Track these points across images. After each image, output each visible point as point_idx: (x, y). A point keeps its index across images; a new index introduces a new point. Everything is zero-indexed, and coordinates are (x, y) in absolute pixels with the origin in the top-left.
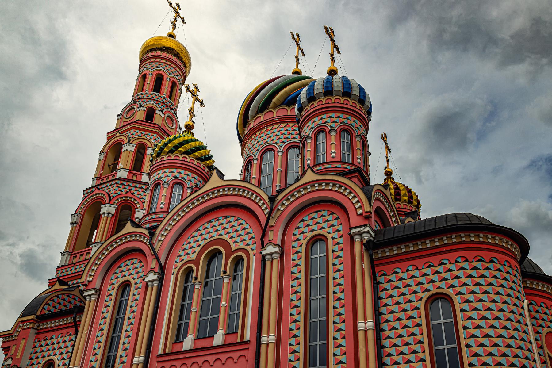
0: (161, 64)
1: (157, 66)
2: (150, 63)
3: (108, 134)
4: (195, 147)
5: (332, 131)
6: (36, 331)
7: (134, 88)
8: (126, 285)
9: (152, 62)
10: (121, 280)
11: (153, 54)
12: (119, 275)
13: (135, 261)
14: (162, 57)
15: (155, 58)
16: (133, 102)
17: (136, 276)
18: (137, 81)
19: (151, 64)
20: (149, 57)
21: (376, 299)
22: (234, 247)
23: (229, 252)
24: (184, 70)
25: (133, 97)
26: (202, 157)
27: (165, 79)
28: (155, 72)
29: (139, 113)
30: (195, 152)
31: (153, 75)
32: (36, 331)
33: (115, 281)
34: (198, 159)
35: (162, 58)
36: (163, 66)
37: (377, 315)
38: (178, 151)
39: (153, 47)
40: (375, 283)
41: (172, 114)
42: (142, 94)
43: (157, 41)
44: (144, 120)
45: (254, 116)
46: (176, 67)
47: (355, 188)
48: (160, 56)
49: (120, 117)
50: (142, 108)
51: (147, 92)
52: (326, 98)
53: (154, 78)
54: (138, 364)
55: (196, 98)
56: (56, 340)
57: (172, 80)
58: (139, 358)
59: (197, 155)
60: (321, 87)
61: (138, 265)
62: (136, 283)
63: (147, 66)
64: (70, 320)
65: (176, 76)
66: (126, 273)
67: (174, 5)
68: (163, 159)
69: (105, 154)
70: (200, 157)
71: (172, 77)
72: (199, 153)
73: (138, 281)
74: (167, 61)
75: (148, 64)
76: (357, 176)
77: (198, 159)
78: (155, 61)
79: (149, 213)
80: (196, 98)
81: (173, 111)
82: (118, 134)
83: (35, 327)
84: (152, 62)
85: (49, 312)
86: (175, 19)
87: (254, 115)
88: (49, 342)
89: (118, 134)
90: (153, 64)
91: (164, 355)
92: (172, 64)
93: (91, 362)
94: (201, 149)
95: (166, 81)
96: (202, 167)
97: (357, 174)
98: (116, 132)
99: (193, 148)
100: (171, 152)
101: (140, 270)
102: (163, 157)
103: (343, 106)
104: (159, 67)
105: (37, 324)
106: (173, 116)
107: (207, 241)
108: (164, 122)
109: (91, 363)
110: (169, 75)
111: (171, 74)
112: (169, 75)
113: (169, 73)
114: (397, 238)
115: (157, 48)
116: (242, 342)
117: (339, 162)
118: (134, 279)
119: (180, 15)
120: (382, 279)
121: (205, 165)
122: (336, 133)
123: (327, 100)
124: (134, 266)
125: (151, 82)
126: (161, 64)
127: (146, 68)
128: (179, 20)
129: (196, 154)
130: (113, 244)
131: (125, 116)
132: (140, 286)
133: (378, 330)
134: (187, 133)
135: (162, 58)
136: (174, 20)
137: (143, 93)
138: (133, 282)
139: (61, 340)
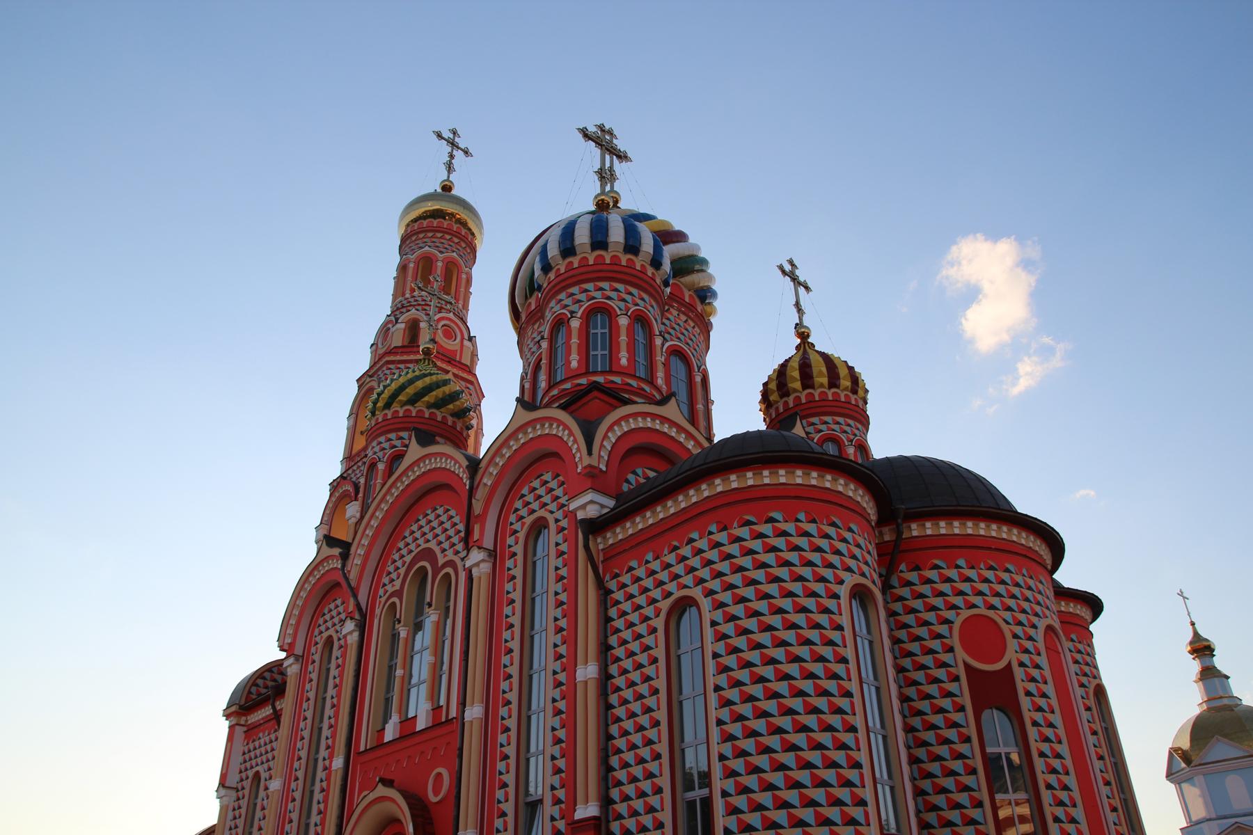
6: (245, 729)
8: (329, 642)
10: (529, 520)
12: (524, 512)
13: (547, 477)
17: (553, 507)
21: (605, 620)
22: (441, 561)
23: (436, 571)
32: (245, 729)
33: (517, 526)
34: (429, 406)
37: (605, 648)
40: (604, 593)
54: (472, 722)
56: (643, 569)
58: (586, 668)
61: (553, 484)
62: (557, 521)
64: (267, 711)
66: (535, 506)
67: (447, 134)
73: (559, 515)
79: (552, 384)
80: (438, 297)
83: (243, 722)
85: (273, 683)
86: (452, 156)
88: (626, 578)
91: (366, 750)
93: (503, 693)
100: (388, 405)
101: (559, 492)
105: (244, 718)
107: (413, 554)
109: (504, 695)
114: (741, 458)
116: (448, 721)
118: (552, 512)
120: (613, 585)
121: (644, 261)
124: (535, 494)
128: (459, 154)
130: (504, 452)
132: (564, 523)
133: (605, 677)
138: (550, 518)
139: (671, 559)
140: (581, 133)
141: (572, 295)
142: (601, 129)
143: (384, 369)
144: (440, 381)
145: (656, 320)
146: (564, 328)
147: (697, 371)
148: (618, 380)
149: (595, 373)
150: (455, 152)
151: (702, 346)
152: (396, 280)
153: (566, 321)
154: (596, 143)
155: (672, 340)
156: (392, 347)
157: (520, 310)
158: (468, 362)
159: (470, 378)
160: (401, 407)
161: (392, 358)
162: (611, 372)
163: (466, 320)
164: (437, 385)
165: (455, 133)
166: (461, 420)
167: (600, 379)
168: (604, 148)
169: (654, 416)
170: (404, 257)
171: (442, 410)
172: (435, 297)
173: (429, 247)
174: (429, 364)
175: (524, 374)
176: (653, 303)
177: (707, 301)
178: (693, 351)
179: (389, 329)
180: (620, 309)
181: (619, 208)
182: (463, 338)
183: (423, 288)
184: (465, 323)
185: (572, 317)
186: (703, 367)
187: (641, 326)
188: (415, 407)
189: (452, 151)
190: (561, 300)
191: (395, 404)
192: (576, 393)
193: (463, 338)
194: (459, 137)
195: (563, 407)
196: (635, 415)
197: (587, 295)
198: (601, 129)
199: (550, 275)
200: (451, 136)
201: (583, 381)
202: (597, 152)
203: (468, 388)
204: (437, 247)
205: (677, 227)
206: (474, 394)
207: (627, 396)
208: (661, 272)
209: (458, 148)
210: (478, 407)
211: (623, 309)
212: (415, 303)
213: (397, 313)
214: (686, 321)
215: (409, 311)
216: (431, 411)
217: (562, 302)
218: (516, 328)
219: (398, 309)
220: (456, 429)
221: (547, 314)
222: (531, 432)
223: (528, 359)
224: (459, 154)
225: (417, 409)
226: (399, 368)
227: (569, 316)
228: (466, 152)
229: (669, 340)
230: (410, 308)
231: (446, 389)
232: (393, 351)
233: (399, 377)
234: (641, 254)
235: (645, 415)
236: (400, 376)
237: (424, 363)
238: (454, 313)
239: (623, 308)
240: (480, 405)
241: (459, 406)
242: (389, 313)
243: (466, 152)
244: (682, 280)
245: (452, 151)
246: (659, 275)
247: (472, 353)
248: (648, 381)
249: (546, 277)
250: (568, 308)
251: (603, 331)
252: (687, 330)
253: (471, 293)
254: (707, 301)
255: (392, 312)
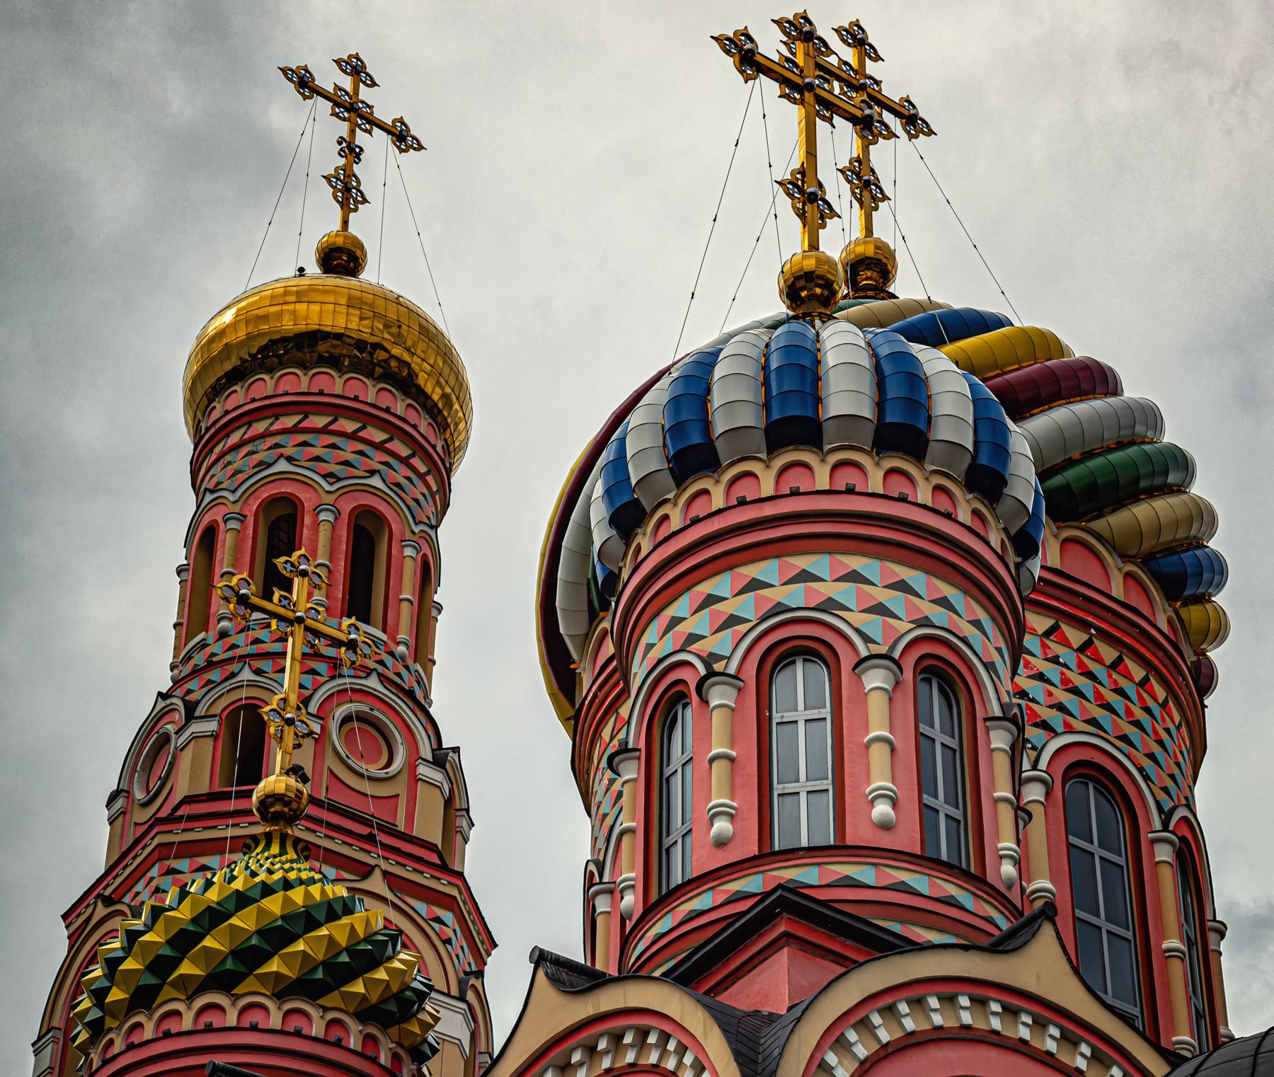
0: (277, 446)
1: (261, 463)
2: (228, 458)
3: (69, 921)
4: (259, 932)
5: (443, 773)
7: (175, 620)
9: (235, 447)
11: (258, 391)
14: (274, 401)
15: (246, 419)
16: (161, 704)
18: (185, 576)
19: (229, 463)
20: (218, 426)
24: (415, 427)
25: (176, 672)
26: (338, 954)
27: (307, 520)
28: (250, 501)
29: (186, 759)
30: (266, 957)
31: (242, 518)
34: (284, 990)
35: (273, 410)
36: (288, 451)
38: (174, 985)
39: (228, 366)
41: (371, 700)
42: (203, 645)
43: (265, 318)
44: (217, 789)
45: (587, 636)
46: (363, 427)
47: (706, 1036)
48: (267, 402)
49: (119, 803)
50: (196, 727)
51: (224, 624)
52: (779, 462)
53: (250, 531)
55: (307, 629)
57: (347, 506)
59: (277, 974)
60: (748, 393)
63: (215, 480)
65: (372, 473)
67: (329, 78)
68: (136, 1039)
69: (60, 1035)
70: (298, 979)
71: (345, 493)
72: (287, 960)
74: (306, 417)
75: (220, 464)
76: (786, 935)
77: (284, 990)
78: (272, 428)
80: (307, 629)
81: (373, 683)
82: (101, 911)
84: (235, 447)
86: (352, 151)
87: (582, 630)
89: (101, 911)
90: (238, 460)
92: (335, 420)
94: (321, 916)
95: (316, 525)
96: (317, 1029)
97: (782, 928)
98: (87, 907)
99: (249, 938)
102: (177, 1014)
103: (769, 510)
104: (270, 465)
106: (378, 705)
108: (330, 762)
110: (327, 488)
111: (339, 479)
112: (327, 488)
113: (328, 476)
115: (244, 361)
117: (755, 858)
119: (378, 114)
122: (734, 692)
123: (787, 475)
125: (236, 563)
126: (277, 446)
127: (212, 492)
128: (375, 144)
129: (274, 965)
131: (139, 795)
134: (275, 849)
135: (273, 410)
136: (342, 161)
137: (211, 636)
140: (728, 52)
141: (711, 600)
142: (854, 36)
143: (154, 872)
144: (318, 906)
145: (990, 667)
146: (689, 712)
147: (1157, 825)
148: (864, 873)
149: (792, 854)
150: (361, 138)
151: (1179, 743)
152: (187, 576)
153: (693, 687)
154: (783, 81)
155: (1070, 730)
156: (178, 797)
157: (575, 656)
158: (429, 827)
159: (443, 886)
160: (190, 999)
161: (178, 836)
162: (841, 849)
163: (427, 696)
164: (308, 920)
165: (355, 68)
166: (394, 1030)
167: (807, 875)
168: (809, 97)
169: (981, 990)
170: (209, 497)
171: (331, 1000)
172: (299, 630)
173: (290, 459)
174: (283, 851)
175: (592, 867)
176: (981, 615)
177: (1188, 592)
178: (1147, 764)
179: (165, 739)
180: (867, 639)
181: (894, 296)
182: (414, 758)
183: (256, 600)
184: (422, 709)
185: (711, 673)
186: (1182, 812)
187: (942, 691)
188: (239, 997)
189: (352, 132)
190: (676, 621)
191: (250, 984)
192: (724, 924)
193: (414, 758)
194: (374, 84)
195: (684, 978)
196: (915, 990)
197: (758, 601)
198: (854, 36)
199: (639, 539)
200: (346, 82)
201: (753, 883)
202: (793, 114)
203: (438, 920)
204: (318, 459)
205: (1080, 348)
206: (459, 941)
207: (896, 927)
208: (1004, 506)
209: (374, 123)
210: (472, 981)
211: (879, 639)
212: (252, 649)
213: (193, 684)
214: (1116, 665)
215: (233, 675)
216: (287, 1006)
217: (679, 628)
218: (565, 720)
219: (196, 672)
220: (374, 1061)
221: (635, 669)
222: (606, 1052)
223: (605, 815)
224: (375, 144)
225: (243, 1002)
226: (204, 868)
227: (703, 671)
228: (402, 137)
229: (1060, 729)
230: (234, 667)
231: (338, 931)
232: (180, 812)
233: (180, 902)
234: (933, 450)
235: (948, 987)
236: (184, 894)
237: (268, 846)
238: (383, 678)
239: (876, 634)
240: (480, 974)
241: (388, 984)
242: (166, 685)
243: (402, 137)
244: (1099, 525)
245: (352, 132)
246: (997, 518)
247: (449, 803)
248: (960, 868)
249: (628, 545)
250: (695, 647)
251: (814, 714)
252: (1120, 692)
253: (439, 608)
254: (1188, 592)
255: (176, 682)
